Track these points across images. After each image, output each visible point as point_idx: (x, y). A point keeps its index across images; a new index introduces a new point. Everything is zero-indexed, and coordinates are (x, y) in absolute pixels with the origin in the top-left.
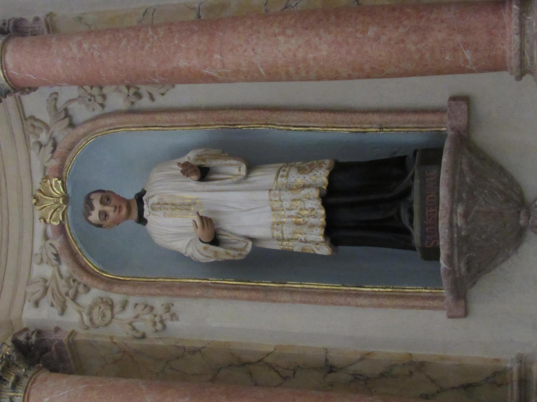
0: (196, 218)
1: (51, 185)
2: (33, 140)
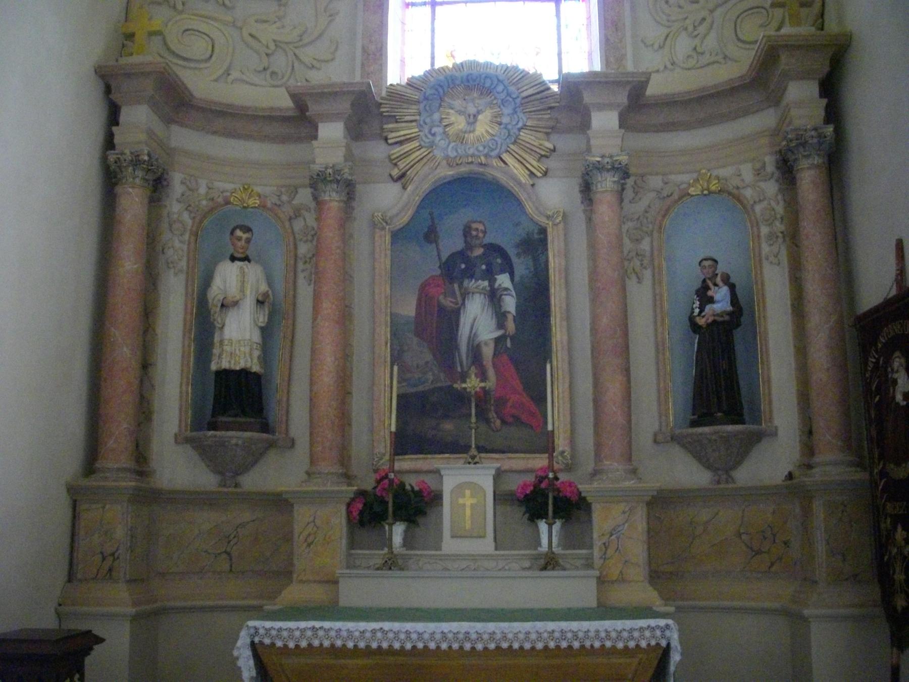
0: (238, 298)
1: (255, 200)
2: (283, 190)
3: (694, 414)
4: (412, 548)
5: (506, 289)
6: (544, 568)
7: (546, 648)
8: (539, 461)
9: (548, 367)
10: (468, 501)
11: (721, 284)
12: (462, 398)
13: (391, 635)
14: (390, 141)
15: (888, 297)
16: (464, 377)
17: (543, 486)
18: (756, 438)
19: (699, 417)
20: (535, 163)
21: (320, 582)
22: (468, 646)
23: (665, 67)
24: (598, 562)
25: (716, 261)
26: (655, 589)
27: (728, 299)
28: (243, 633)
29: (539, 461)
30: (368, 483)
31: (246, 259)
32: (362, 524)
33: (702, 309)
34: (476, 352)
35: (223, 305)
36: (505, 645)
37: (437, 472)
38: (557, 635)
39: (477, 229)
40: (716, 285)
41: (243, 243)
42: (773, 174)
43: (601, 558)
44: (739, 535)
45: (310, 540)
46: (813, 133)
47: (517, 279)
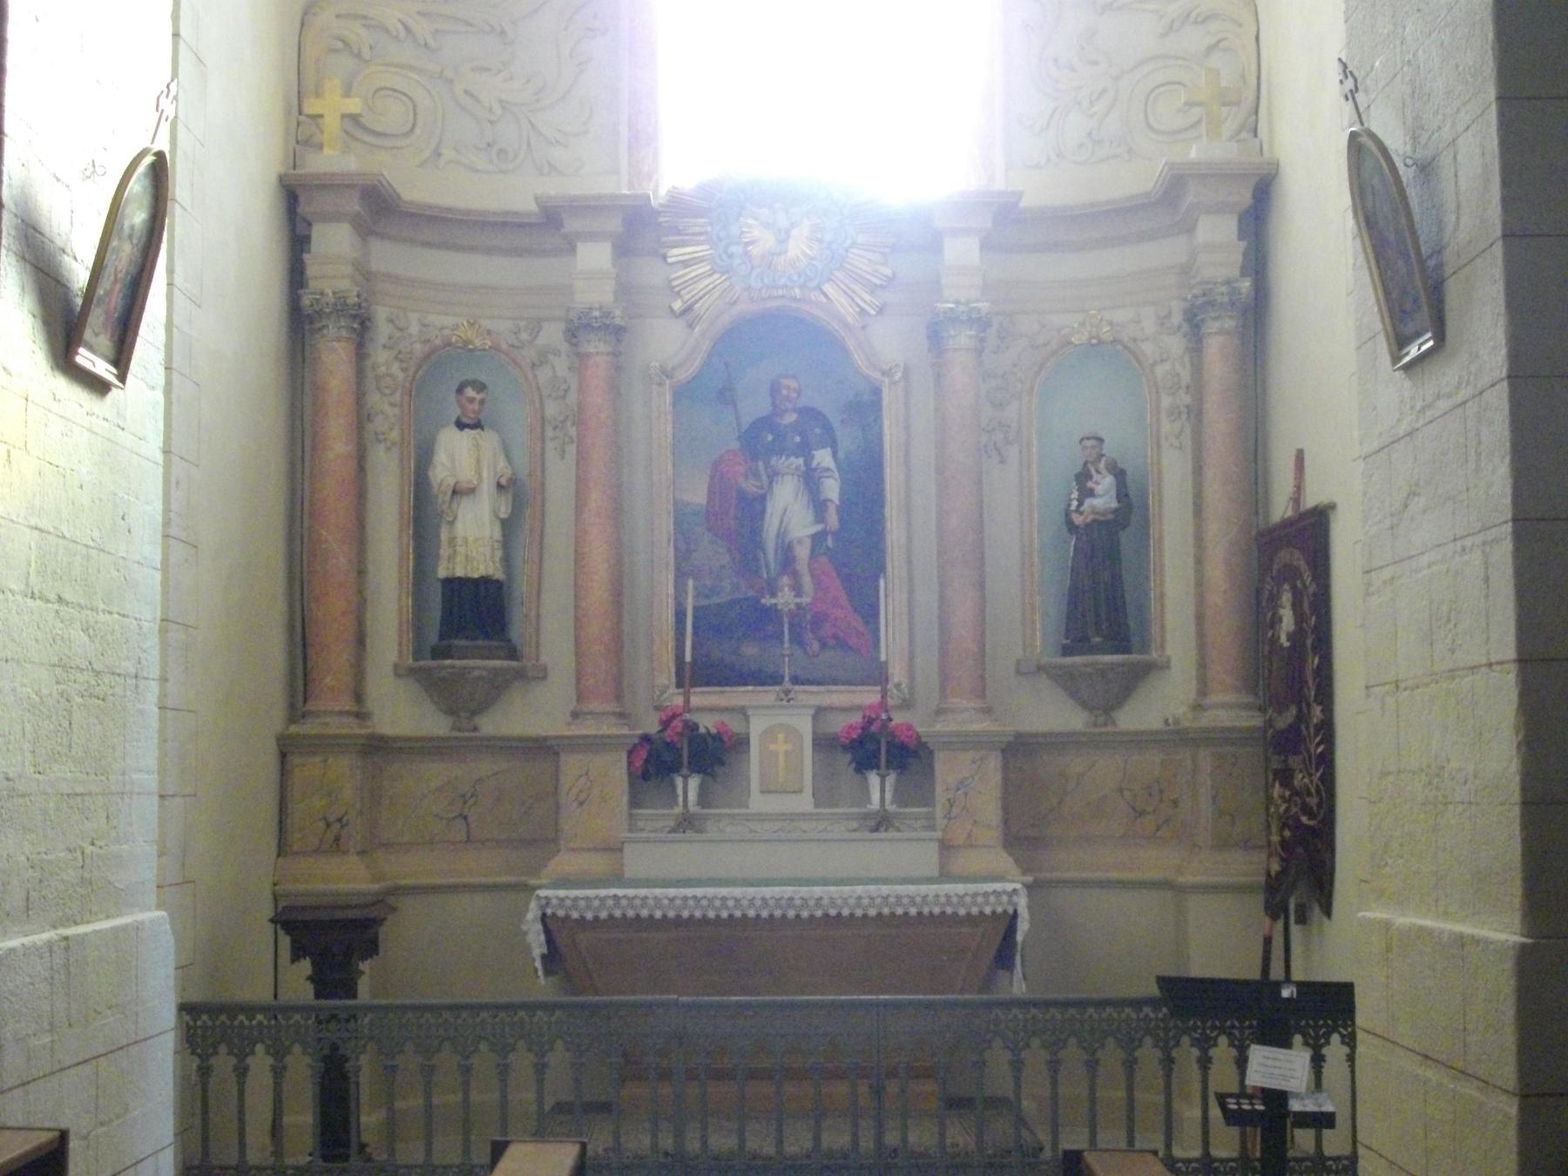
2: (523, 324)
3: (1067, 638)
4: (709, 807)
5: (828, 470)
6: (876, 829)
7: (880, 915)
8: (868, 696)
9: (882, 583)
10: (781, 747)
11: (1104, 472)
12: (771, 614)
13: (704, 902)
14: (670, 260)
15: (1286, 516)
16: (773, 591)
17: (873, 728)
18: (1140, 674)
19: (1072, 641)
20: (867, 297)
21: (595, 849)
22: (791, 914)
23: (1049, 160)
24: (940, 822)
25: (1100, 440)
26: (1010, 854)
27: (1113, 493)
28: (533, 905)
29: (868, 696)
30: (651, 726)
31: (477, 425)
32: (645, 776)
33: (1081, 503)
34: (787, 560)
35: (454, 492)
36: (833, 912)
37: (742, 711)
38: (892, 900)
39: (788, 388)
40: (1098, 472)
41: (476, 406)
42: (1179, 327)
43: (945, 817)
44: (1121, 790)
45: (581, 798)
46: (1224, 289)
47: (841, 455)
